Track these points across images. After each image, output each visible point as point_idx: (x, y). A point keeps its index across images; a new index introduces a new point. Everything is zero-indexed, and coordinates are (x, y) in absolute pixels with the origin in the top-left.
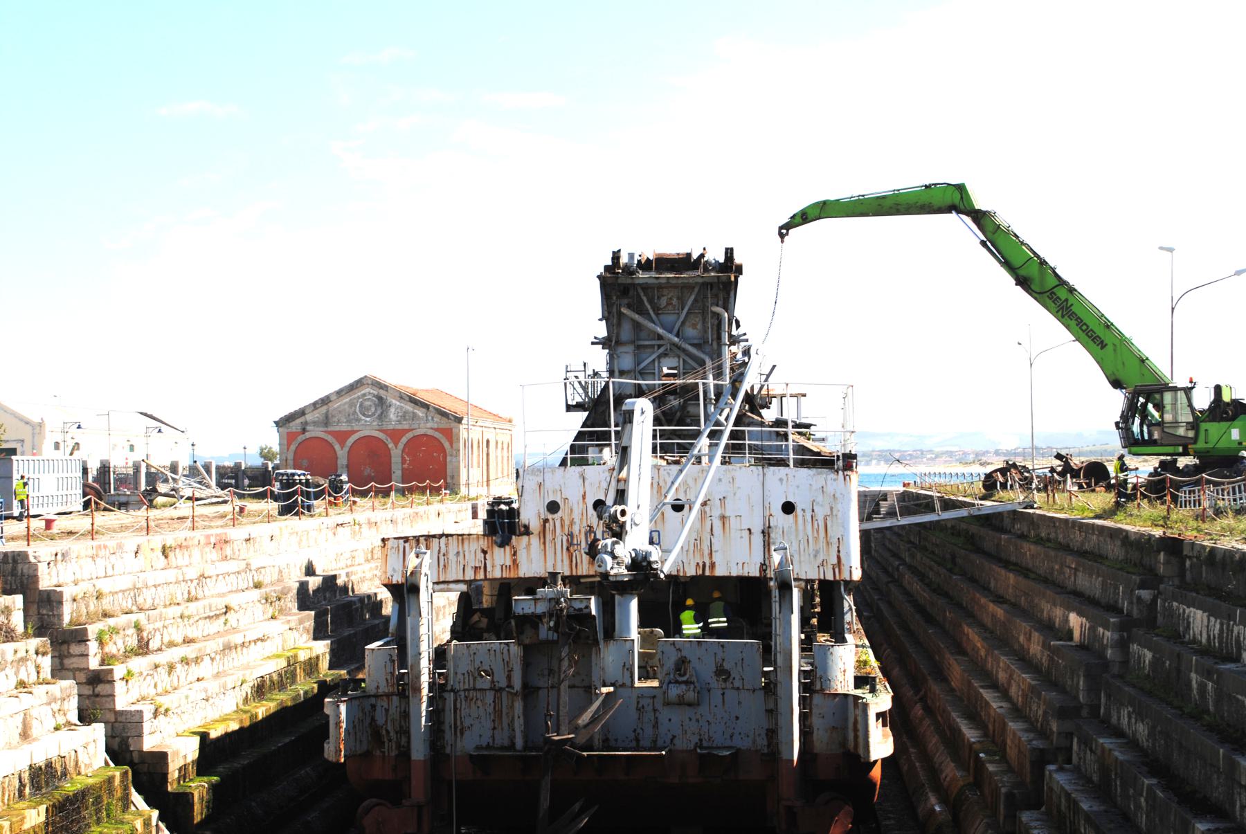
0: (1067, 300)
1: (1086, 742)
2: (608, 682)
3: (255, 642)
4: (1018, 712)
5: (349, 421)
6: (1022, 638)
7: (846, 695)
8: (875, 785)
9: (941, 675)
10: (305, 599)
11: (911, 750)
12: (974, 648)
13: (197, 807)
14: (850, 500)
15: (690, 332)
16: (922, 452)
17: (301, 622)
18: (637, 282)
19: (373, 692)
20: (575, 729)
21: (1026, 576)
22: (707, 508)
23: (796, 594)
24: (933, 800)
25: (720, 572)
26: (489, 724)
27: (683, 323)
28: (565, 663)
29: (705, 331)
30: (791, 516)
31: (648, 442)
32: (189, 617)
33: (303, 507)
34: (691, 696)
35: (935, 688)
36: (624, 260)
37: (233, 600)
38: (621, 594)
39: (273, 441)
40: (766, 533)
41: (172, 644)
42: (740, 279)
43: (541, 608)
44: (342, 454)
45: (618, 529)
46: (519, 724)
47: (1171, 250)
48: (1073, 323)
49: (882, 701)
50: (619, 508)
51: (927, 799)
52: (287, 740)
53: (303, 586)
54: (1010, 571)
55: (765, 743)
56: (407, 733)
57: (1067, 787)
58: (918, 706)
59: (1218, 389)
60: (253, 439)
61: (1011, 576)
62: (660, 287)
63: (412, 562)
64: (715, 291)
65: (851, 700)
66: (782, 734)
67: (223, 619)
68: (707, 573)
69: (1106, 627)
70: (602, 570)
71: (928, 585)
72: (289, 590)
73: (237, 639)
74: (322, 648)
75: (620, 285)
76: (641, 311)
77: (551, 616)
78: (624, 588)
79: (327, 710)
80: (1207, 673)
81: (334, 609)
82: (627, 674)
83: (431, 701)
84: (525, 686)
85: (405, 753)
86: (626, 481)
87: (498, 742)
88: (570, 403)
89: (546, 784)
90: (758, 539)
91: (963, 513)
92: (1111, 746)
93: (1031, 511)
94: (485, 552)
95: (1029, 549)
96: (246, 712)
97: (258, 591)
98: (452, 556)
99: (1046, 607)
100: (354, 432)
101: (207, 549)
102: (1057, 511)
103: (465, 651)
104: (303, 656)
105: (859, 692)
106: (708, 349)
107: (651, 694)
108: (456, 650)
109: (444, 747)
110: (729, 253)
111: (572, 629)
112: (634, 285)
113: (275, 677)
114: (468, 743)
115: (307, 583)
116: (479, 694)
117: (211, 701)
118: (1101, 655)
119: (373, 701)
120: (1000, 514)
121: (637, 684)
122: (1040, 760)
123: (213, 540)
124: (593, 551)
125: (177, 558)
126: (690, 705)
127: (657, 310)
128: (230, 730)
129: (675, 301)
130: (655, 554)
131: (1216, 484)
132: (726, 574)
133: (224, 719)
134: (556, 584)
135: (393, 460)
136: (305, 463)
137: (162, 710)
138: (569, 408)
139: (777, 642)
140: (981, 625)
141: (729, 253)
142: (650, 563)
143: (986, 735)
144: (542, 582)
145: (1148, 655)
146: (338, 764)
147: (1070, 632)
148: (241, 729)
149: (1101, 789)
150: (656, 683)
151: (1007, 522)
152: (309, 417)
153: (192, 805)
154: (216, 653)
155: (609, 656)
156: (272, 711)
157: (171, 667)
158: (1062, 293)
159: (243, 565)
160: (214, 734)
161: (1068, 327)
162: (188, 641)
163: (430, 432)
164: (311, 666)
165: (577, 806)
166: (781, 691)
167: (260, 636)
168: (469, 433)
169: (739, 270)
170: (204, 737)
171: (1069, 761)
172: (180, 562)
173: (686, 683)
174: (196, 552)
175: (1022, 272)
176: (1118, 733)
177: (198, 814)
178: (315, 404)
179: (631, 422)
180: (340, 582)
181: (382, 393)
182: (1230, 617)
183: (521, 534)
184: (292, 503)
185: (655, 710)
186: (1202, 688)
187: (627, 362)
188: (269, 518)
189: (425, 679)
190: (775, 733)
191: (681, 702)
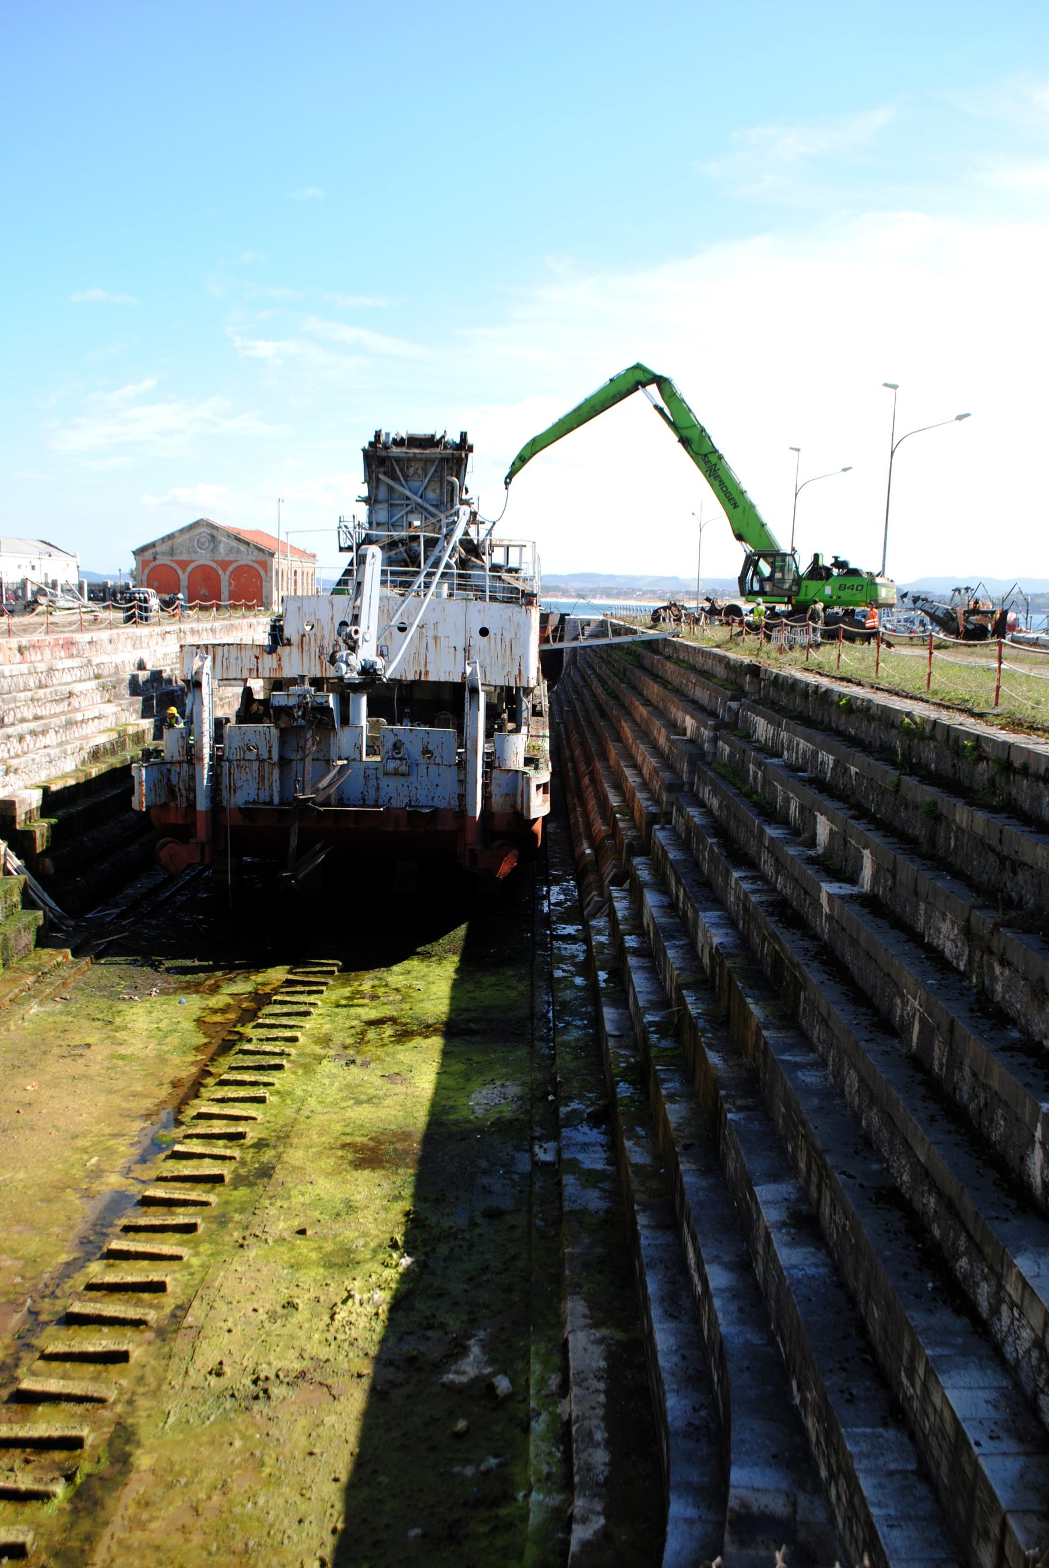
0: (716, 465)
1: (680, 810)
2: (343, 757)
3: (93, 719)
4: (645, 786)
5: (189, 553)
6: (655, 732)
7: (517, 771)
8: (536, 835)
9: (604, 757)
10: (135, 687)
11: (579, 809)
12: (627, 739)
13: (38, 842)
14: (529, 628)
15: (431, 495)
16: (633, 590)
17: (131, 704)
18: (391, 455)
19: (168, 759)
20: (316, 791)
21: (665, 687)
22: (424, 630)
23: (482, 696)
24: (585, 845)
25: (432, 678)
26: (255, 786)
27: (426, 488)
28: (310, 743)
29: (442, 495)
30: (486, 638)
31: (378, 577)
32: (38, 700)
33: (141, 619)
34: (403, 768)
35: (599, 765)
36: (383, 438)
37: (77, 688)
38: (354, 693)
39: (131, 563)
40: (467, 650)
41: (23, 720)
42: (470, 455)
43: (292, 701)
44: (184, 578)
45: (352, 644)
46: (276, 786)
47: (798, 450)
48: (717, 483)
49: (544, 776)
50: (354, 628)
51: (582, 844)
52: (115, 792)
53: (134, 679)
54: (656, 682)
55: (457, 803)
56: (194, 790)
57: (663, 842)
58: (587, 778)
59: (816, 557)
60: (118, 566)
61: (656, 686)
62: (409, 460)
63: (197, 663)
64: (450, 464)
65: (520, 774)
66: (469, 798)
67: (66, 703)
68: (423, 679)
69: (706, 728)
70: (339, 674)
71: (606, 690)
72: (123, 680)
73: (79, 717)
74: (147, 724)
75: (378, 457)
76: (395, 478)
77: (299, 707)
78: (357, 688)
79: (134, 773)
80: (759, 765)
81: (162, 695)
82: (357, 751)
83: (211, 767)
84: (281, 758)
85: (192, 805)
86: (360, 608)
87: (261, 799)
88: (342, 545)
89: (295, 829)
90: (460, 654)
91: (628, 638)
92: (694, 814)
93: (675, 639)
94: (257, 658)
95: (670, 667)
96: (82, 771)
97: (97, 681)
98: (232, 660)
99: (673, 710)
100: (193, 561)
101: (56, 649)
102: (693, 640)
103: (238, 732)
104: (131, 730)
105: (526, 769)
106: (443, 508)
107: (375, 767)
108: (230, 731)
109: (221, 802)
110: (464, 436)
111: (314, 717)
112: (389, 457)
113: (108, 746)
114: (239, 799)
115: (137, 676)
116: (247, 763)
117: (54, 763)
118: (701, 748)
119: (169, 766)
120: (657, 640)
121: (364, 758)
122: (653, 819)
123: (61, 642)
124: (333, 660)
125: (34, 656)
126: (403, 775)
127: (406, 477)
128: (68, 785)
129: (420, 471)
130: (380, 664)
131: (792, 627)
132: (437, 680)
133: (65, 776)
134: (303, 684)
135: (222, 583)
136: (156, 584)
137: (12, 769)
138: (341, 549)
139: (468, 730)
140: (634, 721)
141: (464, 436)
142: (375, 670)
143: (624, 801)
144: (293, 681)
145: (727, 749)
146: (141, 811)
147: (685, 729)
148: (78, 785)
149: (684, 843)
150: (378, 759)
151: (661, 646)
152: (158, 549)
153: (35, 840)
154: (59, 727)
155: (343, 739)
156: (104, 771)
157: (21, 738)
158: (713, 459)
159: (85, 661)
160: (54, 788)
161: (712, 485)
162: (37, 718)
163: (251, 563)
164: (139, 737)
165: (318, 846)
166: (469, 767)
167: (97, 715)
168: (279, 563)
169: (471, 449)
170: (46, 790)
171: (670, 822)
172: (33, 658)
173: (401, 759)
174: (47, 652)
175: (686, 433)
176: (701, 804)
177: (40, 846)
178: (163, 539)
179: (364, 563)
180: (164, 675)
181: (214, 532)
182: (779, 725)
183: (284, 645)
184: (135, 612)
185: (377, 778)
186: (755, 774)
187: (382, 516)
188: (111, 625)
189: (206, 752)
190: (463, 798)
191: (396, 773)
